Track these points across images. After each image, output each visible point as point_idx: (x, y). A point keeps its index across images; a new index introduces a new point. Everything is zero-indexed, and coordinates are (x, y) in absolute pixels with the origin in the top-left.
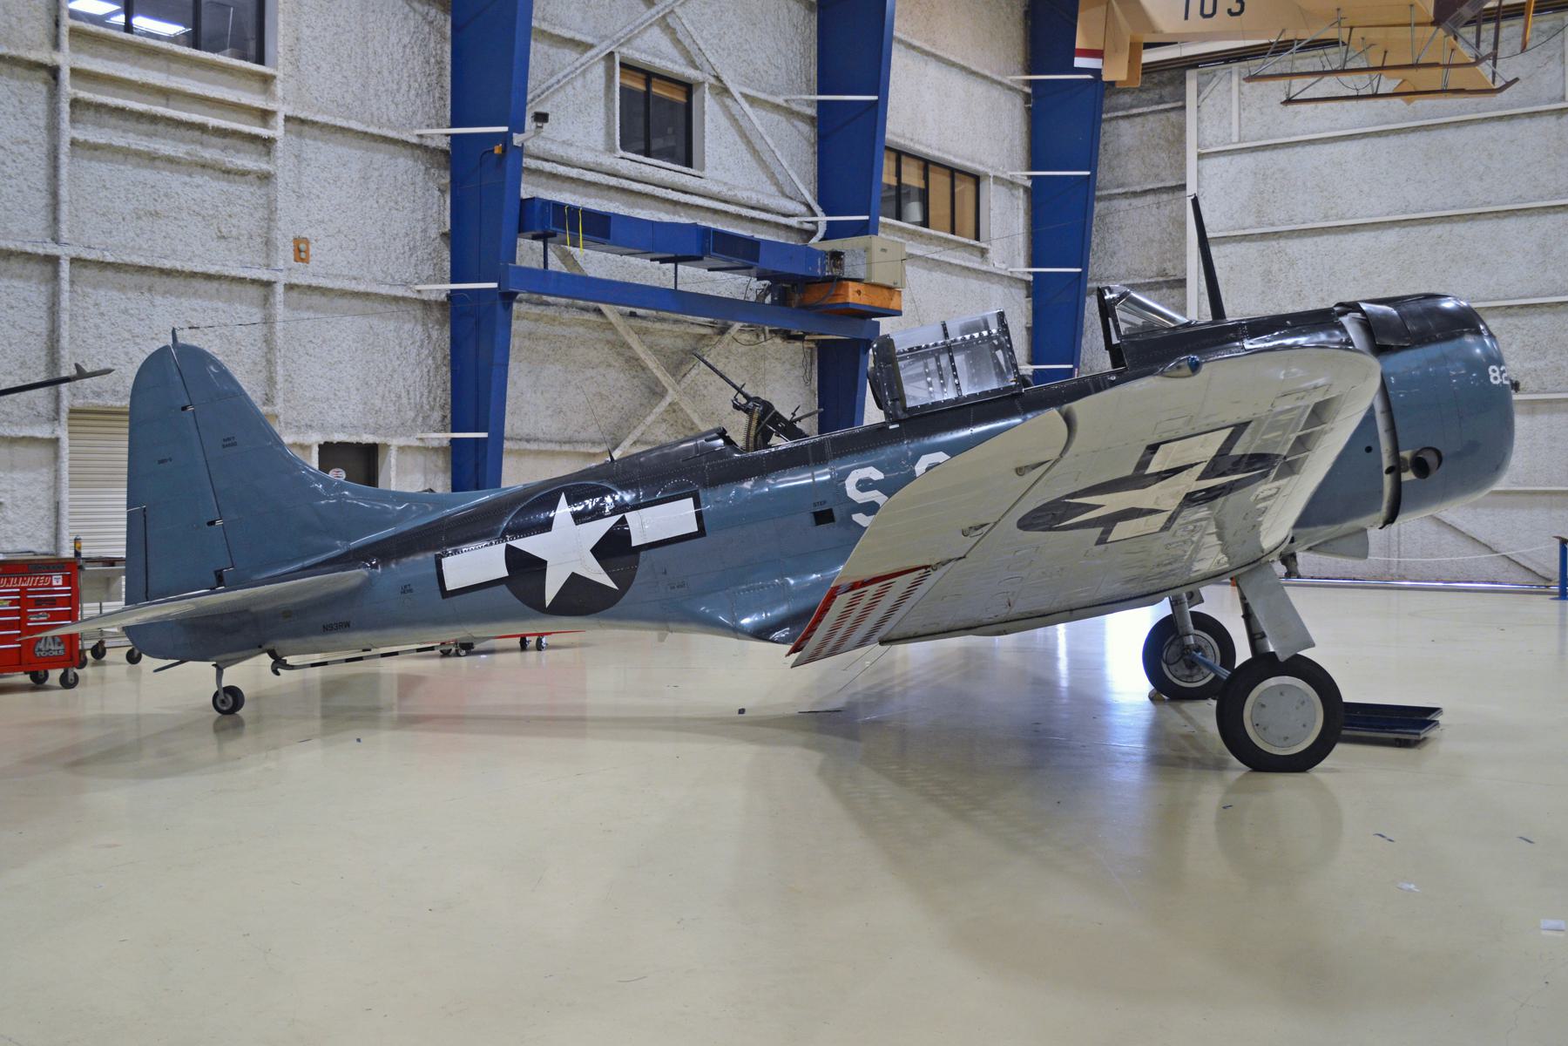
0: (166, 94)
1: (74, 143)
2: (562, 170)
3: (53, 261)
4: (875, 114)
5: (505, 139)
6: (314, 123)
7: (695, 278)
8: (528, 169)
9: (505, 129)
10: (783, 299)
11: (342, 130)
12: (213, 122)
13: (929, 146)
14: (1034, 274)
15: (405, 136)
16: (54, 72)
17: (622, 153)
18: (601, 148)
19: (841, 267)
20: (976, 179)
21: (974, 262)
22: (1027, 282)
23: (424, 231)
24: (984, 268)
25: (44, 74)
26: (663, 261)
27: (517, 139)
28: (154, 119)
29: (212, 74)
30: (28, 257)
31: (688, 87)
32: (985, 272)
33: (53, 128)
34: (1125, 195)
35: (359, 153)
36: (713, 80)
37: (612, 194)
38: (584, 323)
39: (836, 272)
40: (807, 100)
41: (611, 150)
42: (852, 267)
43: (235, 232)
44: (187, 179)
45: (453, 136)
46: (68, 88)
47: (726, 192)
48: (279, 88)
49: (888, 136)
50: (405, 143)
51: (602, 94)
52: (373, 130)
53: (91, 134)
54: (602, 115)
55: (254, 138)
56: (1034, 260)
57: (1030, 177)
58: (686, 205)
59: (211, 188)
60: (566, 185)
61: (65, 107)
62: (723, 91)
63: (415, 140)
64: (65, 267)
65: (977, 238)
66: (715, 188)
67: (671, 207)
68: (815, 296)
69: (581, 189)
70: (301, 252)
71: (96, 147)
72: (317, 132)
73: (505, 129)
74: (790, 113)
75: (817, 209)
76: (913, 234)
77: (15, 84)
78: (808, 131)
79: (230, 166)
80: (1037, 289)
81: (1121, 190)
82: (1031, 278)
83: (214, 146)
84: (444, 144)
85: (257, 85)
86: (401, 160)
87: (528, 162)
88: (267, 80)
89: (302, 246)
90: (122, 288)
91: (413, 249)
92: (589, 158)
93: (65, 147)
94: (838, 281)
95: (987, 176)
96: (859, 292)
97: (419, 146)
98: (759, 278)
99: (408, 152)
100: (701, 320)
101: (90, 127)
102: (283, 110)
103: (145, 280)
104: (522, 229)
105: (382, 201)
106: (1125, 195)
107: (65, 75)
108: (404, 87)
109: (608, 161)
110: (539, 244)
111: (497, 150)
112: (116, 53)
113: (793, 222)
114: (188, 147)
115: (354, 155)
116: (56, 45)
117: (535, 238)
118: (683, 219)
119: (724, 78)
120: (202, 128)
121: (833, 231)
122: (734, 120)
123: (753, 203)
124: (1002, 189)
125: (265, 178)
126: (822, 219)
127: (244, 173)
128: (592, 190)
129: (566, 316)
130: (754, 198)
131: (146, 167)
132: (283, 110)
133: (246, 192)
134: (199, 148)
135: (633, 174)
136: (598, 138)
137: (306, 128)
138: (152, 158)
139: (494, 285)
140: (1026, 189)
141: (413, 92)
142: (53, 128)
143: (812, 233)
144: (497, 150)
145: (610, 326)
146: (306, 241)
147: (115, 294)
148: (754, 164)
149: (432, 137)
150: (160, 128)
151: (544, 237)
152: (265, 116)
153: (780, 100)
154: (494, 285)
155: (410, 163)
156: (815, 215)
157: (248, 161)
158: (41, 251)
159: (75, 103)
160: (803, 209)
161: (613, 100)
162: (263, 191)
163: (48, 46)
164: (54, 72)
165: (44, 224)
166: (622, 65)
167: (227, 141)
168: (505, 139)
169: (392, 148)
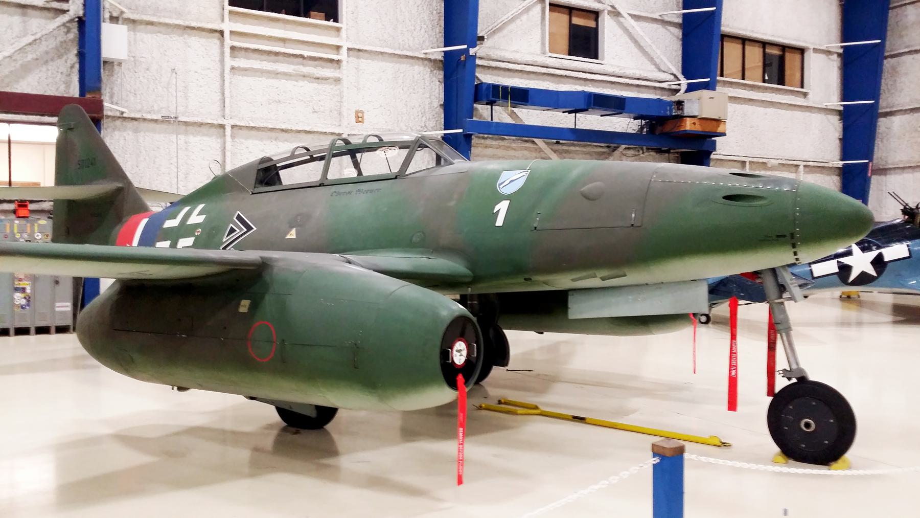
0: (284, 40)
1: (233, 68)
2: (511, 66)
3: (222, 126)
4: (714, 19)
5: (466, 51)
6: (366, 51)
7: (592, 121)
8: (479, 66)
9: (465, 47)
10: (652, 130)
11: (382, 53)
12: (306, 53)
13: (765, 34)
14: (844, 106)
15: (417, 54)
16: (222, 33)
17: (550, 55)
18: (539, 52)
19: (682, 109)
20: (802, 51)
21: (799, 101)
22: (839, 111)
23: (431, 103)
24: (805, 104)
25: (218, 35)
26: (570, 112)
27: (472, 51)
28: (277, 54)
29: (300, 28)
30: (212, 125)
31: (595, 14)
32: (807, 107)
33: (222, 61)
34: (910, 52)
35: (392, 65)
36: (610, 9)
37: (546, 77)
38: (526, 149)
39: (679, 113)
40: (836, 46)
41: (544, 53)
42: (688, 109)
43: (322, 109)
44: (296, 83)
45: (445, 52)
46: (229, 41)
47: (618, 71)
48: (343, 33)
49: (723, 28)
50: (418, 58)
51: (539, 22)
52: (399, 52)
53: (241, 62)
54: (540, 31)
55: (331, 61)
56: (845, 96)
57: (842, 47)
58: (592, 80)
59: (307, 87)
60: (516, 74)
61: (227, 50)
62: (615, 13)
63: (423, 56)
64: (228, 130)
65: (802, 87)
66: (610, 70)
67: (583, 82)
68: (668, 128)
69: (525, 76)
70: (359, 118)
71: (246, 70)
72: (366, 55)
73: (465, 47)
74: (664, 22)
75: (681, 76)
76: (792, 92)
77: (203, 41)
78: (678, 32)
79: (318, 76)
80: (846, 115)
81: (907, 50)
82: (842, 108)
83: (309, 66)
84: (440, 57)
85: (334, 33)
86: (416, 67)
87: (478, 62)
88: (805, 95)
89: (360, 115)
90: (261, 139)
91: (423, 114)
92: (529, 58)
93: (227, 70)
94: (681, 118)
95: (808, 48)
96: (694, 124)
97: (426, 59)
98: (635, 119)
99: (420, 62)
100: (603, 145)
101: (243, 60)
102: (345, 45)
103: (273, 134)
104: (477, 99)
105: (405, 89)
106: (910, 52)
107: (227, 34)
108: (418, 28)
109: (542, 60)
110: (489, 107)
111: (463, 58)
112: (256, 21)
113: (665, 85)
114: (296, 67)
115: (389, 67)
116: (223, 20)
117: (487, 104)
118: (579, 88)
119: (617, 6)
120: (302, 57)
121: (691, 88)
122: (626, 30)
123: (637, 76)
124: (822, 56)
125: (338, 80)
126: (684, 82)
127: (326, 79)
128: (532, 76)
129: (514, 145)
130: (638, 74)
131: (273, 78)
132: (345, 45)
133: (327, 88)
134: (301, 67)
135: (557, 66)
136: (537, 47)
137: (361, 53)
138: (276, 74)
139: (461, 131)
140: (839, 55)
141: (423, 30)
142: (222, 61)
143: (677, 91)
144: (463, 58)
145: (541, 150)
146: (362, 112)
147: (257, 142)
148: (640, 54)
149: (432, 53)
150: (280, 58)
151: (491, 103)
152: (338, 48)
153: (656, 16)
154: (461, 131)
155: (422, 68)
156: (64, 12)
157: (327, 72)
158: (215, 122)
159: (233, 48)
160: (672, 77)
161: (545, 25)
162: (338, 87)
163: (219, 21)
164: (222, 33)
165: (219, 109)
166: (551, 4)
167: (316, 63)
168: (466, 51)
169: (411, 61)
